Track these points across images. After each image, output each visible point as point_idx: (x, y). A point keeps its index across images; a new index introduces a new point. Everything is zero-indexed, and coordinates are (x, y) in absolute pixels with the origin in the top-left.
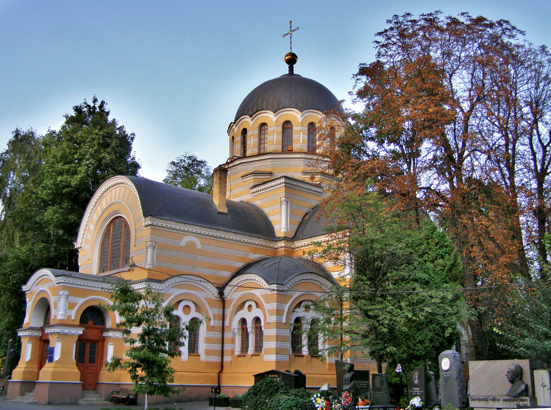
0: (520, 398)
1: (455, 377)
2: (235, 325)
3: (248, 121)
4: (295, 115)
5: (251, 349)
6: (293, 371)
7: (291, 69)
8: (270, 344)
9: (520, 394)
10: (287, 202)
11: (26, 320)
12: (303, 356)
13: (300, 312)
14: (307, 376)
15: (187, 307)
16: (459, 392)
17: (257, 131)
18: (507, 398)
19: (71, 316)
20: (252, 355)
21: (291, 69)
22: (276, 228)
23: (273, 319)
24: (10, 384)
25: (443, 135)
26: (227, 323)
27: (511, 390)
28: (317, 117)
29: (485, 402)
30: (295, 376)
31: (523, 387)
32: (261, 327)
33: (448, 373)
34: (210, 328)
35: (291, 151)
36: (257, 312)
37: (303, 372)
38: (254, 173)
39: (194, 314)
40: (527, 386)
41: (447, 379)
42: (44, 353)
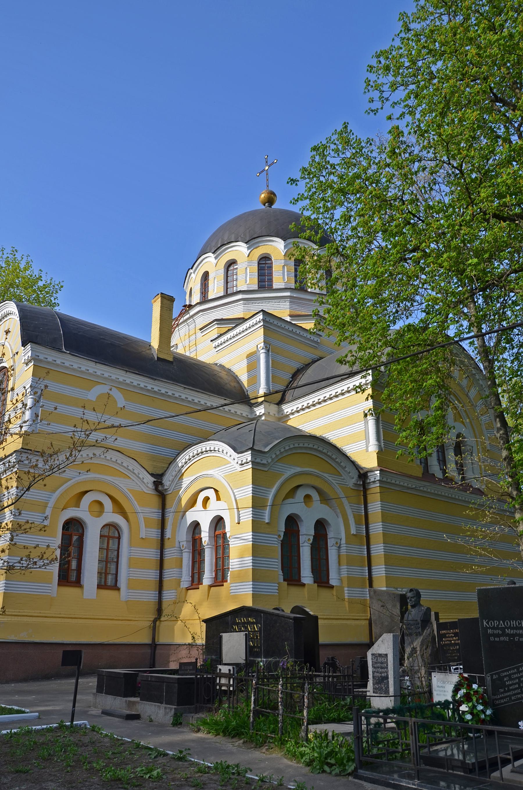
2: (183, 537)
5: (207, 578)
6: (287, 610)
10: (268, 351)
12: (332, 587)
13: (295, 506)
14: (319, 617)
26: (168, 534)
30: (295, 619)
36: (216, 508)
39: (110, 516)
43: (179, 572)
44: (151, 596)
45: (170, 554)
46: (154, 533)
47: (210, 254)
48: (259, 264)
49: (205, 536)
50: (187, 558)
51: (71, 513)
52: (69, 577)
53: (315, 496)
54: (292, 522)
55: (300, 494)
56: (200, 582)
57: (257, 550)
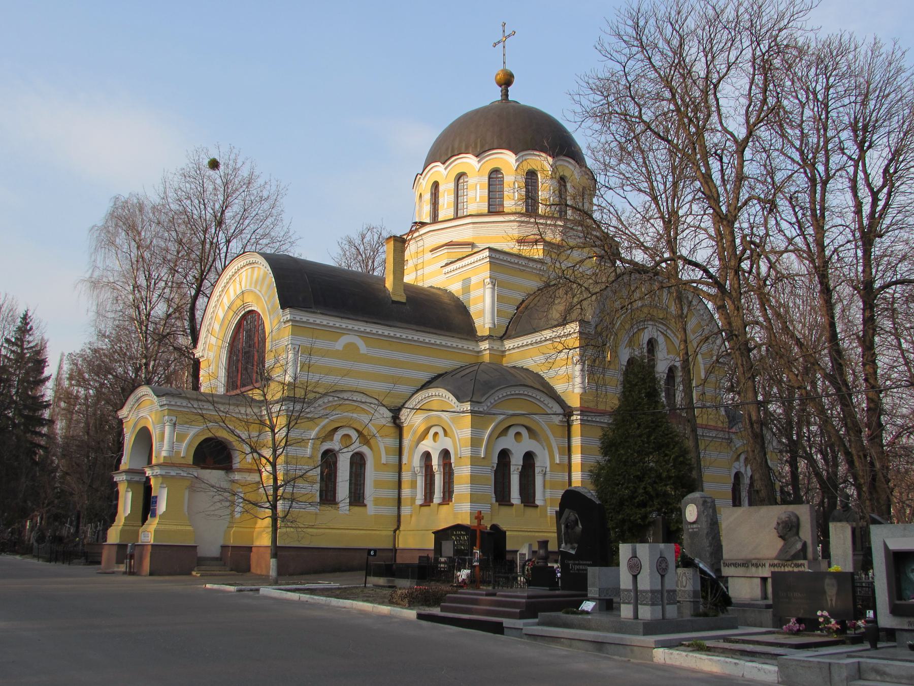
0: (795, 562)
1: (705, 532)
2: (417, 462)
3: (439, 171)
4: (506, 160)
7: (505, 94)
8: (462, 488)
9: (795, 557)
11: (124, 460)
12: (537, 506)
13: (507, 442)
15: (347, 436)
16: (711, 554)
17: (452, 185)
18: (776, 562)
19: (180, 453)
20: (440, 504)
21: (505, 94)
22: (478, 323)
23: (467, 452)
24: (106, 547)
25: (707, 178)
26: (405, 460)
27: (783, 551)
28: (543, 162)
29: (743, 569)
31: (799, 546)
32: (451, 464)
33: (695, 526)
34: (379, 466)
35: (501, 213)
37: (503, 527)
38: (450, 244)
40: (805, 545)
41: (693, 535)
42: (147, 505)
43: (413, 491)
44: (392, 511)
45: (406, 476)
46: (394, 460)
47: (439, 164)
48: (489, 178)
49: (435, 462)
50: (420, 482)
51: (327, 446)
52: (328, 496)
53: (524, 432)
54: (504, 455)
55: (512, 432)
56: (431, 500)
57: (474, 479)
